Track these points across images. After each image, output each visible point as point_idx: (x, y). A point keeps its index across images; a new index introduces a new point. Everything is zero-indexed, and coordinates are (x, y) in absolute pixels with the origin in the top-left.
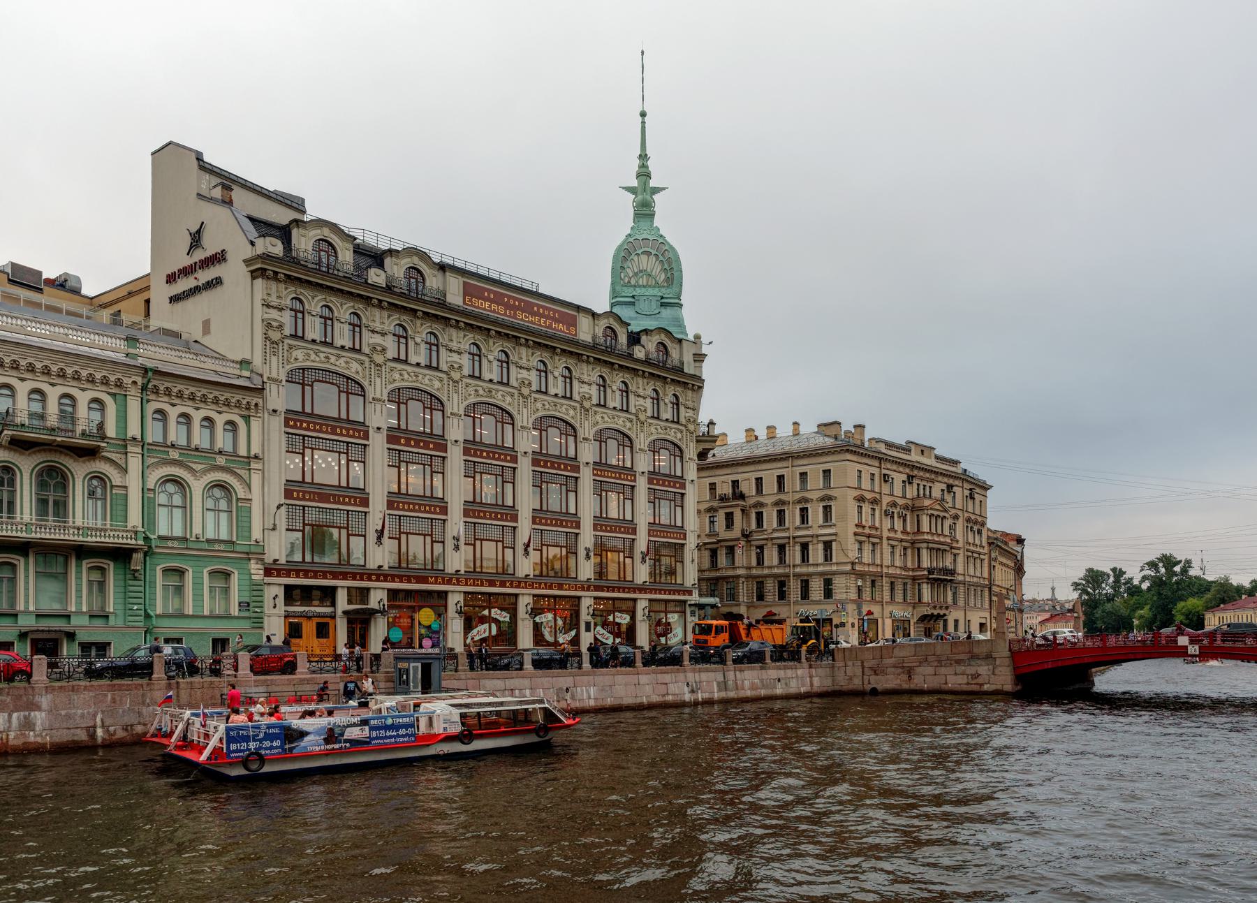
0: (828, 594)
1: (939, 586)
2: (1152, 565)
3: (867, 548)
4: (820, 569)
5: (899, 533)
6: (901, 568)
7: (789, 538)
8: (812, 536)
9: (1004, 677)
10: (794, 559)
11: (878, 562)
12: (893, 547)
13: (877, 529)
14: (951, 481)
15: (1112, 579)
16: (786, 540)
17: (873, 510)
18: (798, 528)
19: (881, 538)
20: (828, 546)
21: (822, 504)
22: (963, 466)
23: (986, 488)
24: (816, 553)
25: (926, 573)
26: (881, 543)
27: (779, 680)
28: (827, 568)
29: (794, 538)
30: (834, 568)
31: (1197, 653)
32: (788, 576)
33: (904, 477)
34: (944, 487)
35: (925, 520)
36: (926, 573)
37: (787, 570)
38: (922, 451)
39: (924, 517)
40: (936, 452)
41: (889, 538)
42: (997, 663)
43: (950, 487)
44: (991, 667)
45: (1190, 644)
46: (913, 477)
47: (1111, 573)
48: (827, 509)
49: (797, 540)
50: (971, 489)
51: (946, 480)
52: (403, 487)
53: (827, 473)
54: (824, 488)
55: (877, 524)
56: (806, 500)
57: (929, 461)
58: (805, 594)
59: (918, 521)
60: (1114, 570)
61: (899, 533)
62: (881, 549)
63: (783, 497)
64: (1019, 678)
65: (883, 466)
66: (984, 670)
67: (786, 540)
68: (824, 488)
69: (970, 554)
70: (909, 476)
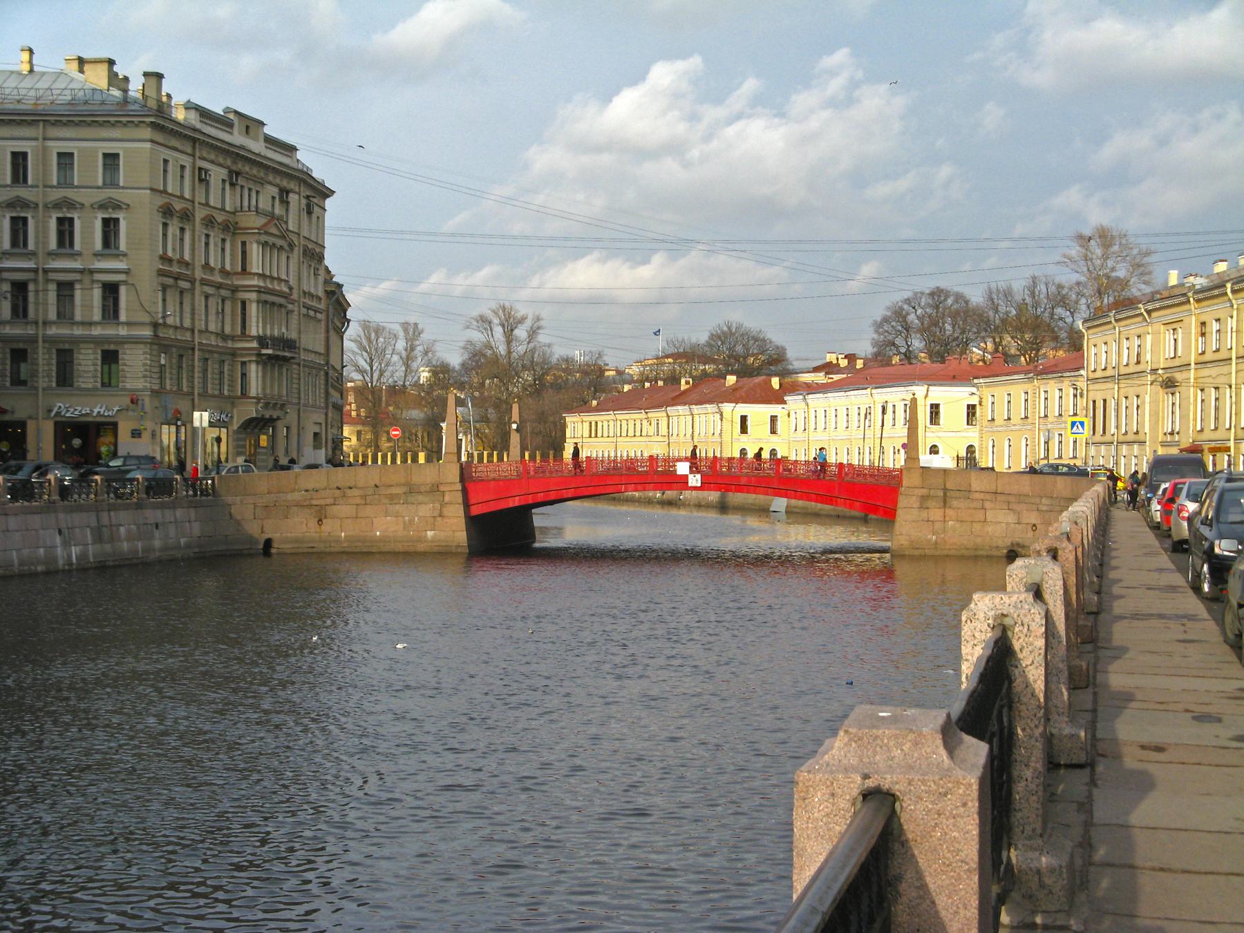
0: (108, 382)
1: (273, 365)
2: (484, 321)
3: (173, 298)
4: (97, 331)
5: (216, 272)
6: (217, 334)
7: (36, 271)
8: (82, 272)
9: (455, 520)
10: (46, 311)
11: (187, 323)
12: (207, 297)
13: (187, 264)
14: (285, 183)
15: (401, 345)
16: (31, 276)
17: (182, 230)
18: (50, 254)
19: (193, 282)
20: (111, 290)
21: (101, 215)
22: (299, 155)
23: (326, 193)
24: (89, 301)
25: (255, 344)
26: (193, 289)
27: (157, 527)
28: (110, 331)
29: (46, 271)
30: (123, 331)
31: (699, 485)
32: (33, 340)
33: (224, 173)
34: (274, 191)
35: (255, 251)
36: (255, 344)
37: (30, 331)
38: (247, 127)
39: (255, 246)
40: (267, 130)
41: (204, 282)
42: (447, 499)
43: (284, 192)
44: (438, 506)
45: (691, 472)
46: (238, 174)
47: (401, 334)
48: (110, 226)
49: (52, 276)
50: (308, 197)
51: (278, 181)
52: (1054, 453)
53: (111, 160)
54: (105, 185)
55: (187, 257)
56: (71, 205)
57: (257, 147)
58: (65, 377)
59: (244, 253)
60: (405, 326)
61: (216, 272)
62: (193, 299)
63: (22, 192)
64: (476, 523)
65: (198, 154)
66: (426, 510)
67: (31, 276)
68: (105, 185)
69: (170, 281)
70: (231, 172)
